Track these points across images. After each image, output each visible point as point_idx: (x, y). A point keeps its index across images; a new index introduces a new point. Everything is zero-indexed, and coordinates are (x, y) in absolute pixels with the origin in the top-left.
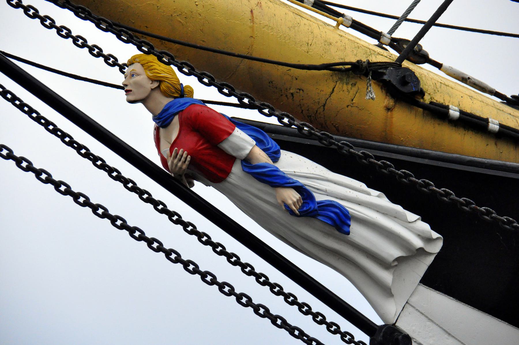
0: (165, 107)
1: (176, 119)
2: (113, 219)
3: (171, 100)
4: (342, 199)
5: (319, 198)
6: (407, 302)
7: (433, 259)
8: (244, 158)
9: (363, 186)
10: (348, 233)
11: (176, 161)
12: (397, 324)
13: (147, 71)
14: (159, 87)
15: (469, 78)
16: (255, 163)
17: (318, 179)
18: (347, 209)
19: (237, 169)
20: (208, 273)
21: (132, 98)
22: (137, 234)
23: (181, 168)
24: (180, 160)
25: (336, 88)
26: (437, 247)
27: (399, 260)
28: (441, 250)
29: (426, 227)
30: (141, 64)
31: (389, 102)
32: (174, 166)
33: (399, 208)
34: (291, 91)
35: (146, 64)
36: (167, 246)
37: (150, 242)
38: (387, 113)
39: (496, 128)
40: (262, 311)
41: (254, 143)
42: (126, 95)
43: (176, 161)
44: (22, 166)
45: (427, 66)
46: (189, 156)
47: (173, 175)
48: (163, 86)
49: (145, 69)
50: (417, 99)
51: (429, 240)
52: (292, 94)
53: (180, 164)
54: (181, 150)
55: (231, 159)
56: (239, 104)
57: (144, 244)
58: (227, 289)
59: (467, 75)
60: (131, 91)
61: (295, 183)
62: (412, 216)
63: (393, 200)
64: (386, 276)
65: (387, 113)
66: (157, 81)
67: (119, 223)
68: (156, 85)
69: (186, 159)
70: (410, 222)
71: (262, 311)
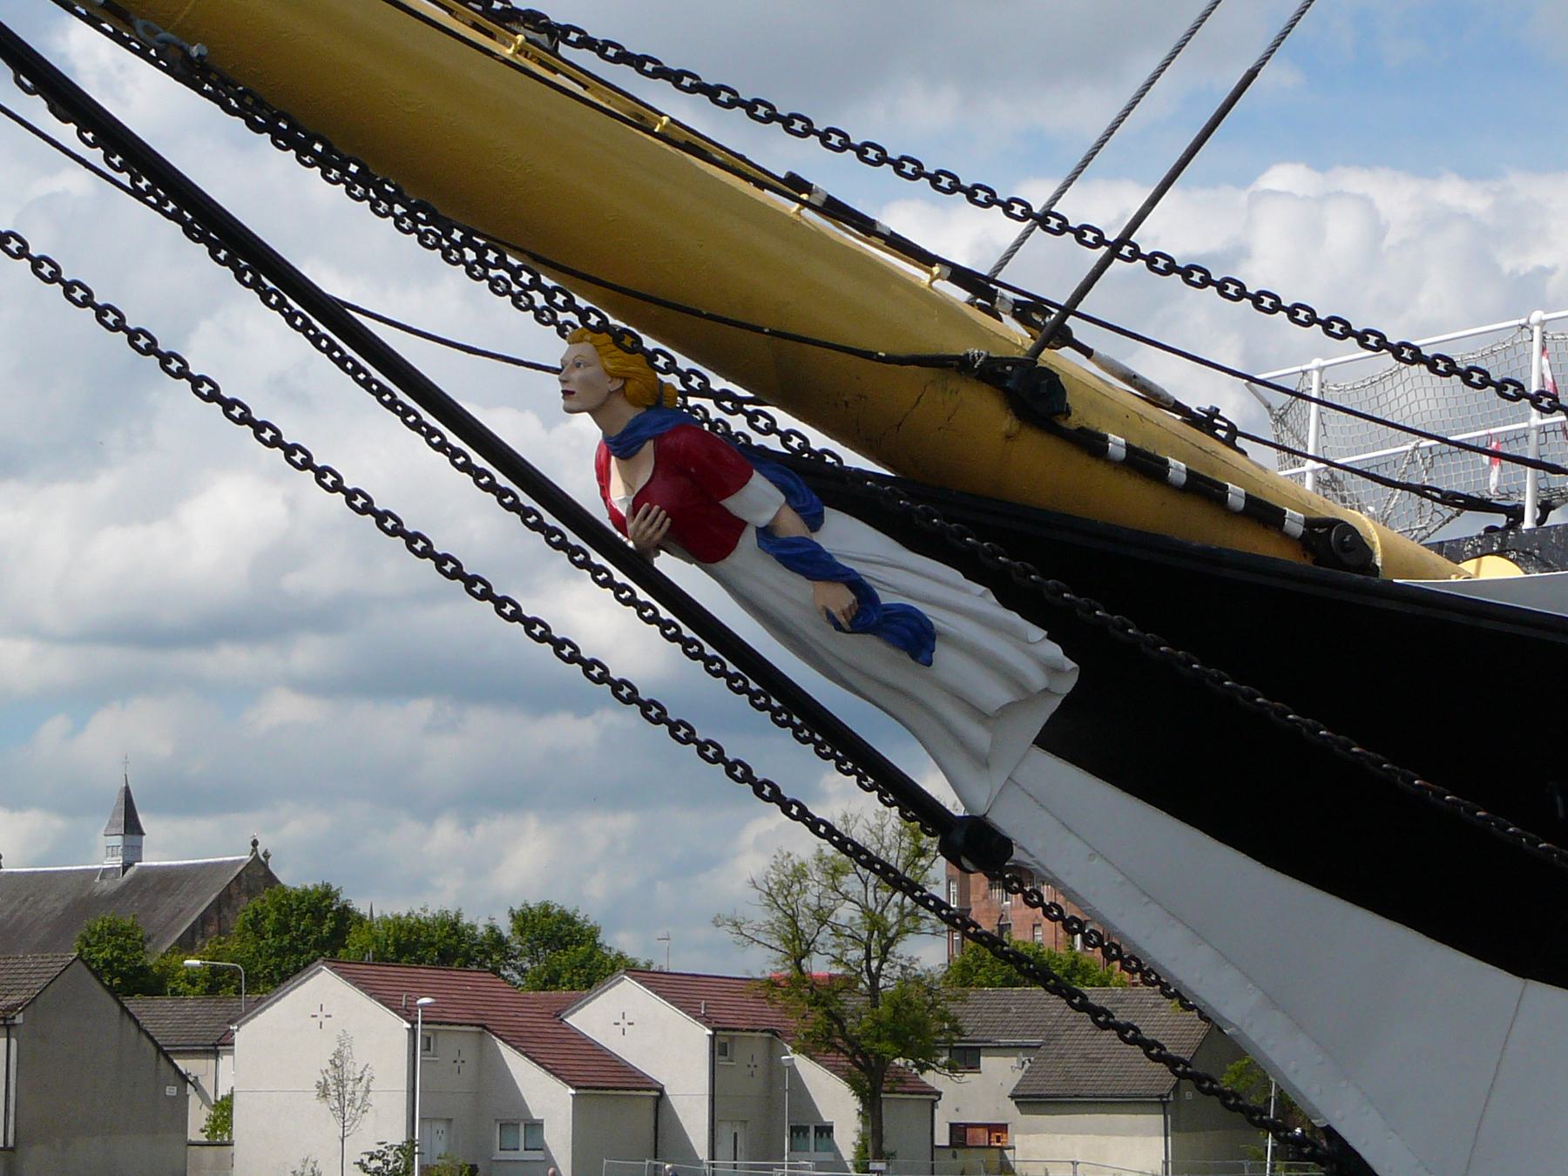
0: (629, 425)
1: (649, 447)
2: (228, 405)
3: (642, 410)
4: (920, 600)
5: (886, 598)
6: (1009, 778)
7: (1059, 703)
8: (763, 525)
9: (955, 575)
10: (929, 663)
11: (644, 525)
12: (987, 816)
13: (604, 359)
14: (623, 387)
15: (1135, 377)
16: (782, 535)
17: (892, 566)
18: (931, 619)
19: (748, 540)
20: (388, 514)
21: (575, 405)
22: (237, 412)
23: (650, 538)
24: (651, 524)
25: (923, 397)
26: (1067, 684)
27: (1006, 709)
28: (1073, 689)
29: (1054, 651)
30: (595, 346)
31: (1008, 423)
32: (638, 534)
33: (1014, 617)
34: (846, 398)
35: (603, 347)
36: (226, 393)
37: (228, 405)
38: (1006, 442)
39: (1183, 478)
40: (767, 791)
41: (782, 498)
42: (563, 398)
43: (644, 525)
44: (385, 527)
45: (1067, 351)
46: (664, 512)
47: (631, 544)
48: (631, 387)
49: (600, 355)
50: (1057, 421)
51: (1053, 670)
52: (846, 404)
53: (650, 531)
54: (656, 507)
55: (740, 525)
56: (543, 274)
57: (216, 408)
58: (682, 732)
59: (1133, 372)
60: (573, 393)
61: (848, 574)
62: (1038, 634)
63: (1006, 601)
64: (979, 735)
65: (1006, 442)
66: (621, 378)
67: (538, 630)
68: (618, 384)
69: (663, 522)
70: (1031, 643)
71: (739, 771)
